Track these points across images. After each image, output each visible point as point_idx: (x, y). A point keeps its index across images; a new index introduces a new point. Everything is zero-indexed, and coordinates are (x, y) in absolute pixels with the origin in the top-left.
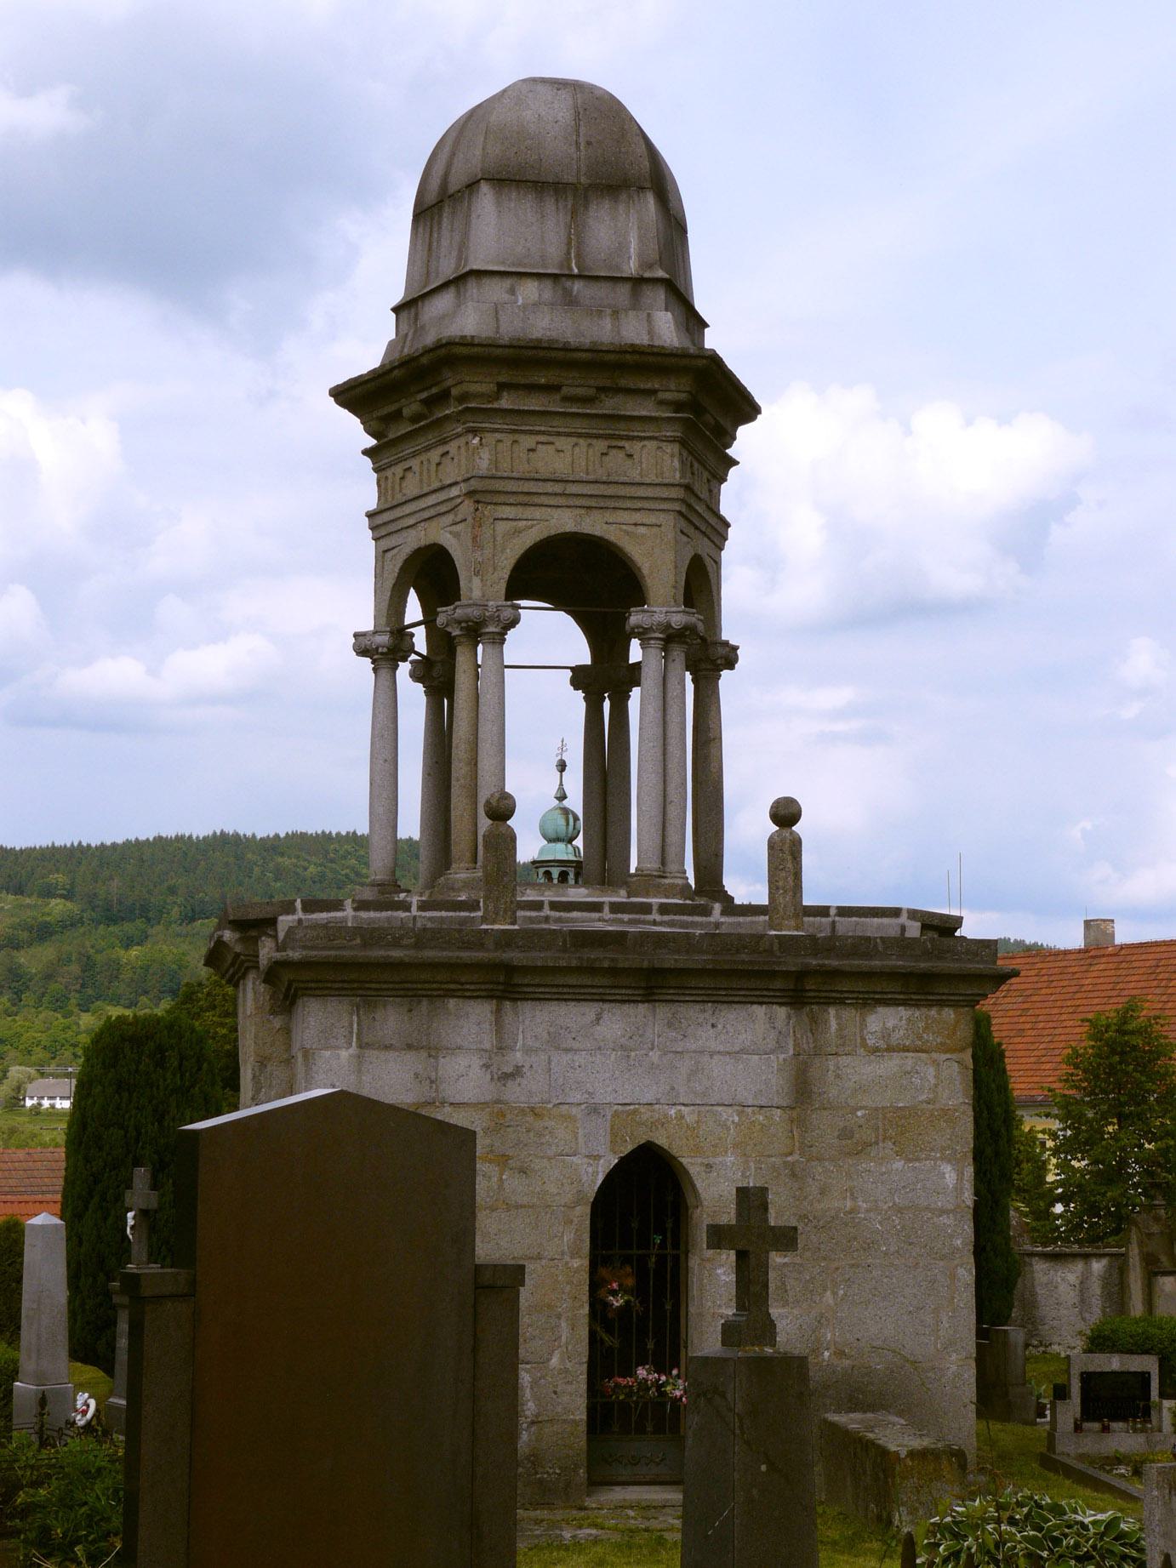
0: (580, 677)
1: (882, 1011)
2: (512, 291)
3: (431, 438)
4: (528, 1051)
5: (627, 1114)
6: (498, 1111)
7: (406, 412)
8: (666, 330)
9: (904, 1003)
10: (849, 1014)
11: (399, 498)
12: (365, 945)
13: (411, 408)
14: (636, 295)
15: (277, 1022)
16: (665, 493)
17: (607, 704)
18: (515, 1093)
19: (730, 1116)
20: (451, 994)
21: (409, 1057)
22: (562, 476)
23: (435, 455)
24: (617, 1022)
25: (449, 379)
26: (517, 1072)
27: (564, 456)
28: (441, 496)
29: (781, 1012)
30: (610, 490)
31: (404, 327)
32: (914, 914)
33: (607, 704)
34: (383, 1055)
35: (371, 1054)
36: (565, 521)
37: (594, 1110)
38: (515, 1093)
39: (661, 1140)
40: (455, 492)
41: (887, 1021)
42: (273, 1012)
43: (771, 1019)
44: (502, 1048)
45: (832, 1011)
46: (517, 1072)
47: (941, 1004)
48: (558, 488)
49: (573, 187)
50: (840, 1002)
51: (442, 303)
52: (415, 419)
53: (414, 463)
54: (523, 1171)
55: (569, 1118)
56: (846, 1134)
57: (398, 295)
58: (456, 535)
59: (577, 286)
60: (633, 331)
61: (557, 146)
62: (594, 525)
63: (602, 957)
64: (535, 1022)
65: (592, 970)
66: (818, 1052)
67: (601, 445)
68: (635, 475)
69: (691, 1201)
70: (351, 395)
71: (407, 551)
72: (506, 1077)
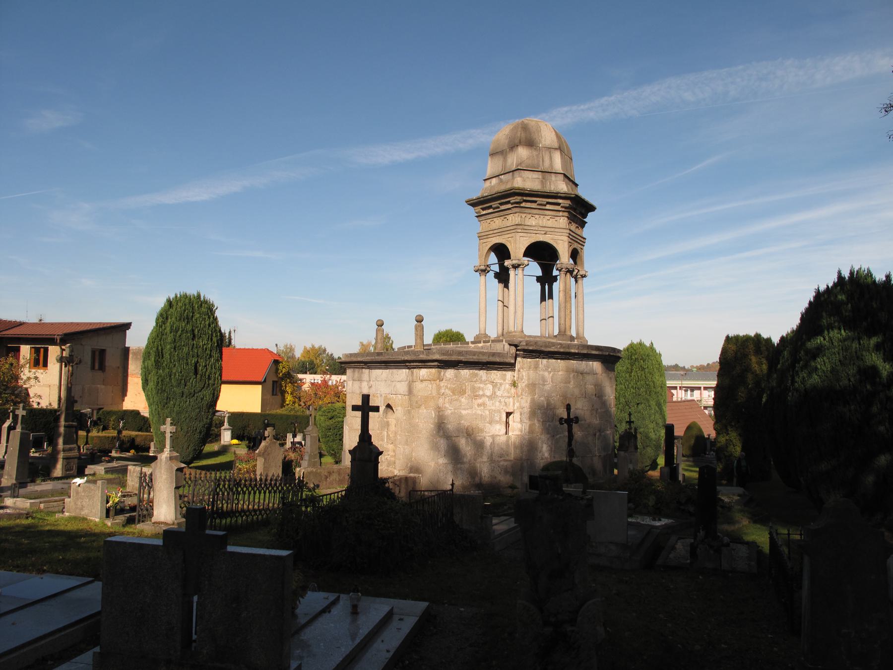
8: (562, 187)
17: (547, 287)
33: (547, 287)
41: (423, 372)
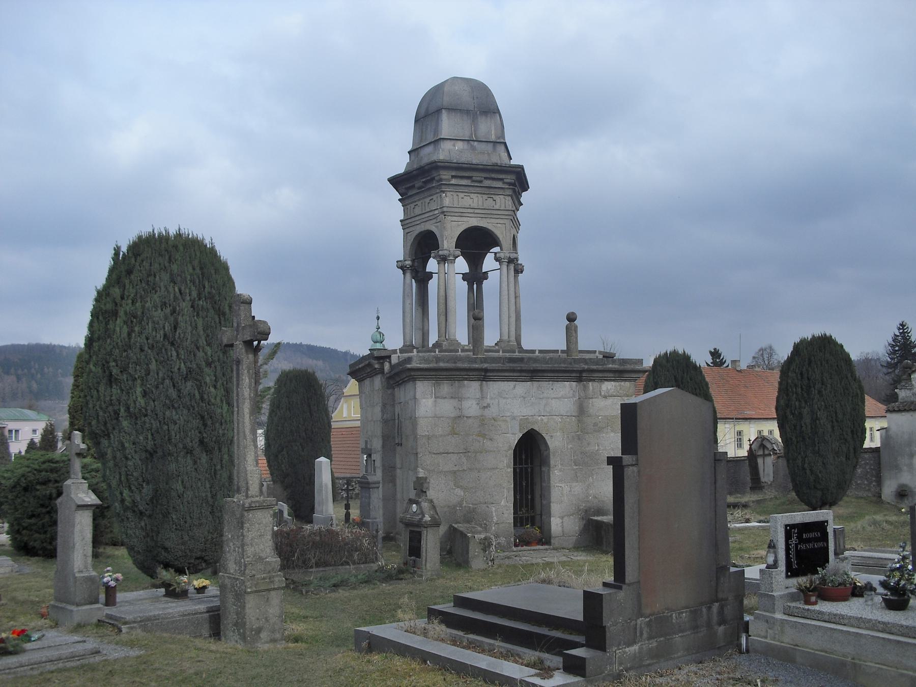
0: (465, 277)
1: (606, 383)
2: (454, 146)
3: (426, 194)
4: (492, 398)
5: (524, 421)
6: (482, 420)
7: (417, 186)
9: (614, 381)
10: (596, 384)
11: (413, 215)
12: (482, 362)
13: (418, 184)
14: (494, 147)
15: (389, 391)
16: (507, 213)
18: (487, 413)
19: (559, 419)
20: (466, 379)
21: (452, 401)
22: (459, 210)
23: (427, 200)
24: (521, 388)
25: (434, 174)
26: (488, 406)
27: (474, 200)
28: (431, 214)
29: (574, 384)
30: (489, 212)
31: (413, 157)
32: (600, 352)
34: (443, 401)
35: (439, 400)
36: (474, 222)
37: (514, 418)
38: (487, 413)
39: (536, 428)
40: (436, 212)
42: (388, 388)
43: (571, 387)
44: (483, 398)
45: (590, 383)
46: (488, 406)
47: (626, 380)
48: (472, 211)
49: (467, 112)
50: (594, 380)
51: (429, 149)
52: (419, 188)
53: (419, 203)
54: (491, 440)
55: (506, 421)
56: (595, 424)
57: (410, 148)
58: (437, 227)
59: (476, 143)
60: (494, 160)
61: (466, 98)
62: (483, 223)
63: (517, 366)
64: (494, 388)
65: (513, 371)
66: (587, 398)
67: (485, 197)
68: (497, 207)
69: (543, 448)
70: (396, 182)
71: (417, 232)
72: (485, 407)
